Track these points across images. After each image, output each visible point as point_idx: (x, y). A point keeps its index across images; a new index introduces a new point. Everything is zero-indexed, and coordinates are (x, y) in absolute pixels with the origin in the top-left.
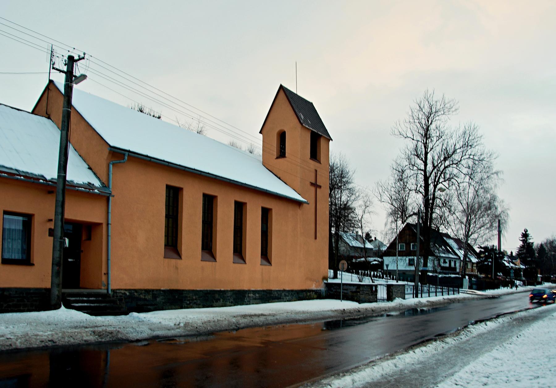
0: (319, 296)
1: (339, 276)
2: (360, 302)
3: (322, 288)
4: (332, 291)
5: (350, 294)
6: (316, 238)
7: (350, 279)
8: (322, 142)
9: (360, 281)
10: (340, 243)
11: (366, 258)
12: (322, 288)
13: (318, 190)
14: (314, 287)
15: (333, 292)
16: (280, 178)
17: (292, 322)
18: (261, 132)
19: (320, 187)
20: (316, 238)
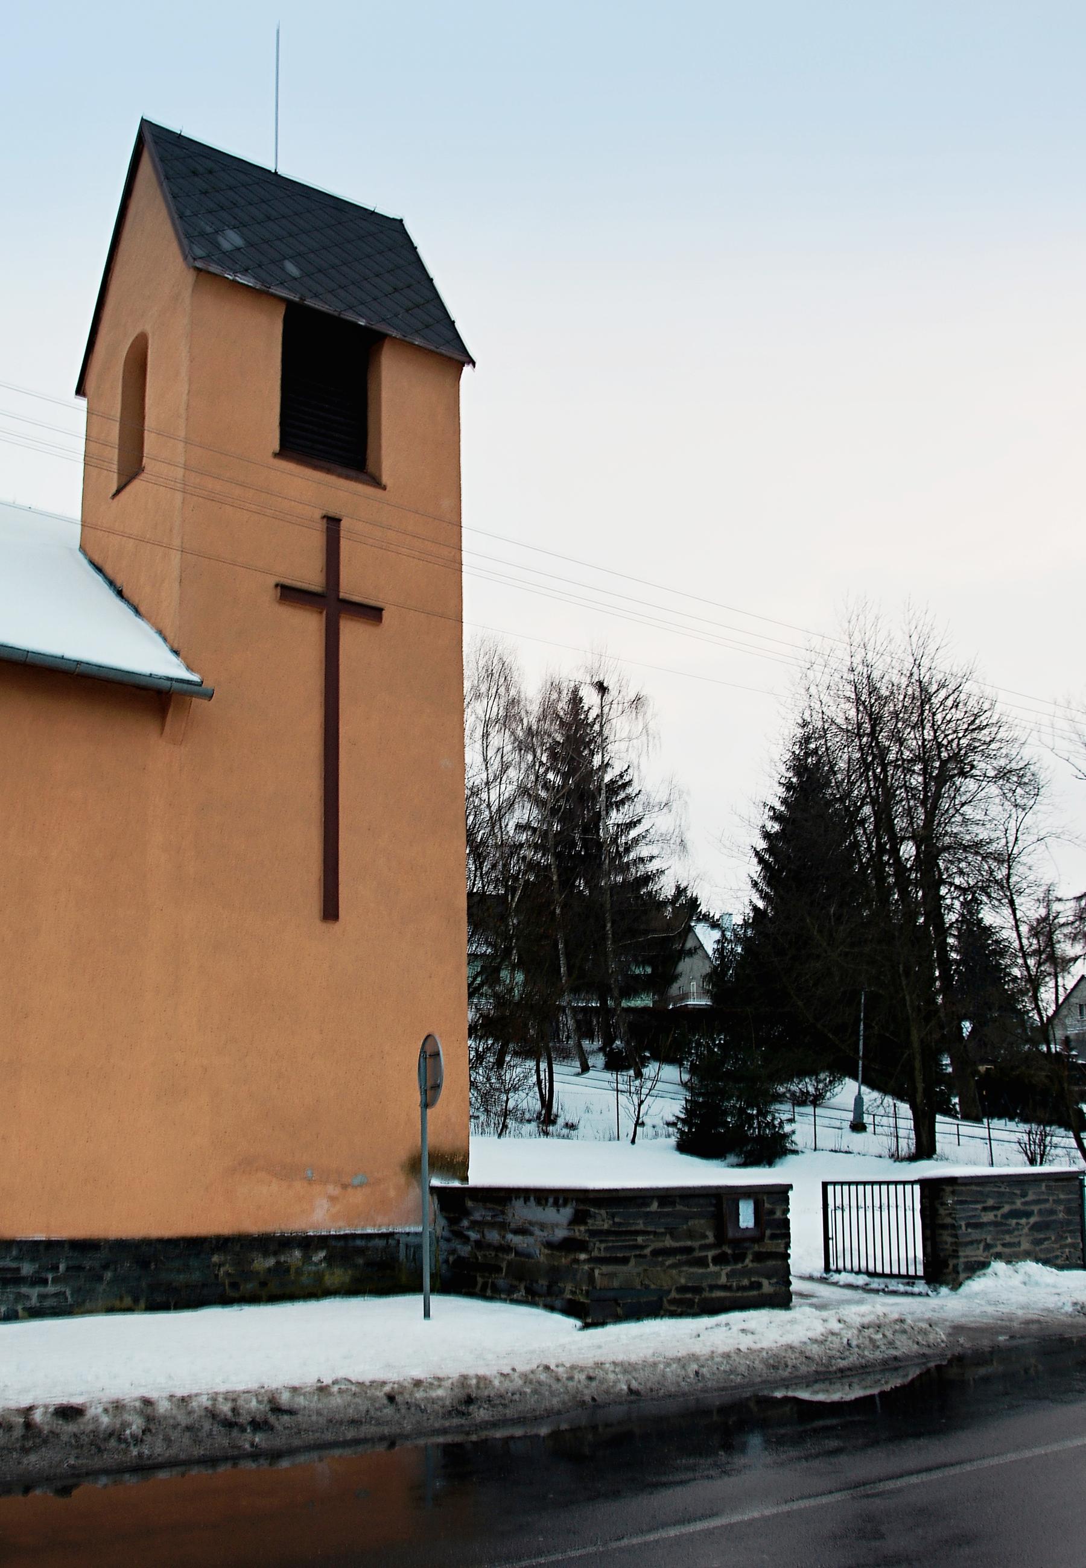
0: (371, 1268)
1: (942, 1142)
2: (591, 1312)
3: (403, 1213)
4: (466, 1239)
5: (541, 1255)
6: (330, 911)
7: (987, 1160)
8: (397, 386)
9: (1032, 1162)
10: (1050, 1012)
11: (587, 1003)
12: (403, 1213)
13: (351, 632)
14: (320, 1216)
15: (481, 1247)
16: (120, 593)
17: (250, 1434)
18: (80, 391)
19: (290, 594)
20: (330, 911)
